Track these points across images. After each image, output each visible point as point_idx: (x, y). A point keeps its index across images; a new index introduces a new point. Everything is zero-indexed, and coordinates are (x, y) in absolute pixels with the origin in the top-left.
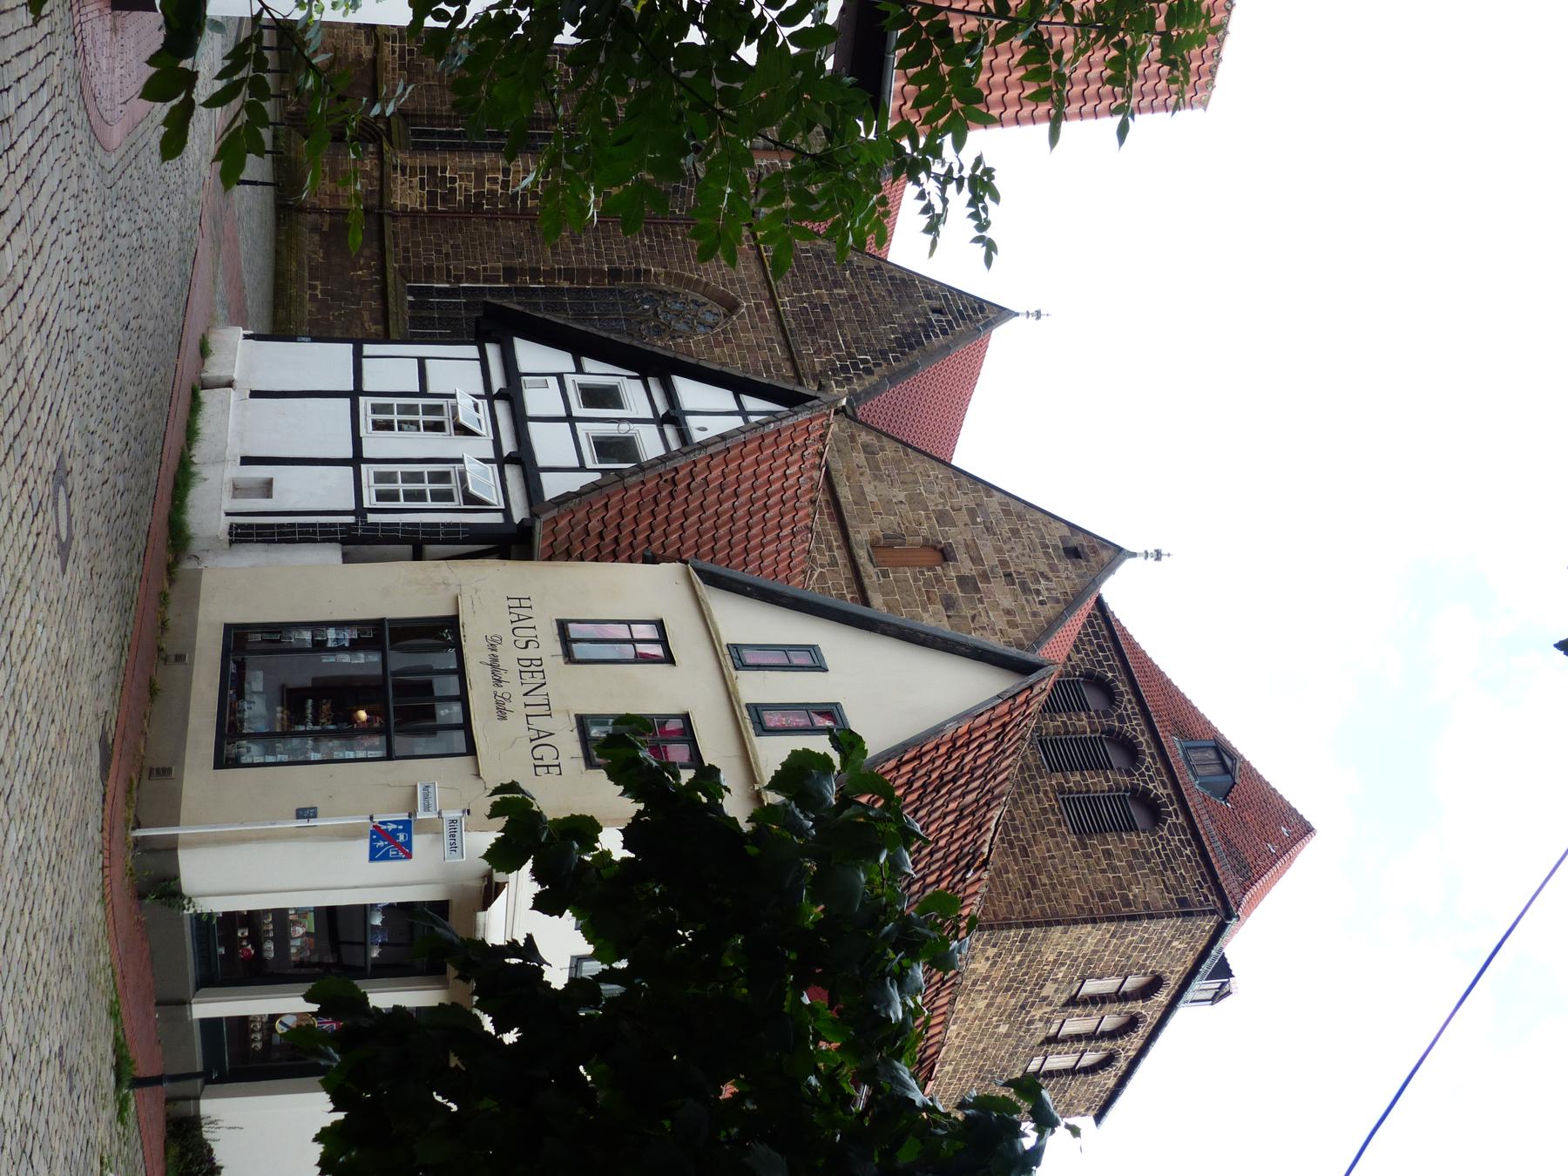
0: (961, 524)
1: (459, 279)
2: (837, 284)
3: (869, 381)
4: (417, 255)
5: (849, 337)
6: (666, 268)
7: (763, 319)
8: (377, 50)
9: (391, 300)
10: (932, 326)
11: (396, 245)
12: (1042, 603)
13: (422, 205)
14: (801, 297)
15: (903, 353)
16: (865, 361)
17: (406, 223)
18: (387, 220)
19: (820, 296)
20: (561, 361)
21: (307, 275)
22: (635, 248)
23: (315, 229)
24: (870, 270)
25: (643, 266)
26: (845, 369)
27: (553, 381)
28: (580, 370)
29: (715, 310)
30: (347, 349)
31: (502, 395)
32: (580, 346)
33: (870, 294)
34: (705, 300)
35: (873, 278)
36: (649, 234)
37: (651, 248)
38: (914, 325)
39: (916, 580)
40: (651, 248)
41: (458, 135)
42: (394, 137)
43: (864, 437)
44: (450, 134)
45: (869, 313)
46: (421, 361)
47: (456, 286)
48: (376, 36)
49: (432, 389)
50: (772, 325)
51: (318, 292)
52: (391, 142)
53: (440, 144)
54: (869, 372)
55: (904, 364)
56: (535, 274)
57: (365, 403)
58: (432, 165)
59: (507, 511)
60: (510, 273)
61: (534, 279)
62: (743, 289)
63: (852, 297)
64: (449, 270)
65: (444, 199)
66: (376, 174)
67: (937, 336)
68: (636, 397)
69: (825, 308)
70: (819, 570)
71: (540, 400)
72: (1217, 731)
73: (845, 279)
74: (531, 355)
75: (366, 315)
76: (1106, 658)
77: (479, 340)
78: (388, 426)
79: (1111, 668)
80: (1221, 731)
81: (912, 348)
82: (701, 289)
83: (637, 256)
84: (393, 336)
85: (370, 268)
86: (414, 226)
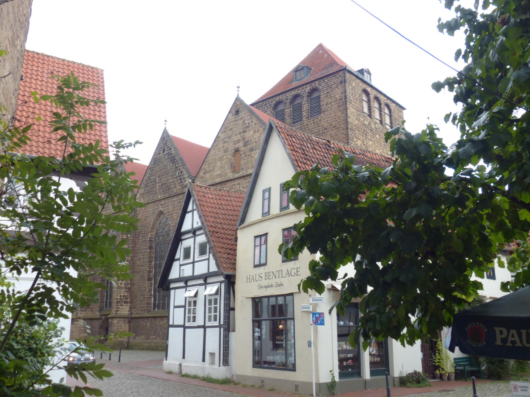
0: (228, 146)
1: (151, 295)
2: (155, 181)
3: (184, 172)
4: (143, 307)
5: (171, 178)
6: (149, 232)
7: (165, 203)
8: (80, 318)
9: (157, 315)
10: (168, 153)
11: (140, 313)
12: (252, 122)
13: (128, 305)
14: (159, 192)
15: (176, 162)
16: (179, 173)
17: (133, 311)
18: (132, 316)
19: (159, 186)
20: (176, 265)
21: (148, 341)
22: (143, 241)
23: (134, 338)
24: (151, 171)
25: (148, 239)
26: (181, 179)
27: (182, 268)
29: (162, 218)
30: (171, 330)
32: (171, 259)
33: (158, 171)
34: (159, 222)
35: (153, 170)
36: (138, 237)
37: (143, 237)
38: (168, 158)
39: (244, 159)
40: (143, 237)
41: (107, 294)
43: (201, 174)
44: (107, 297)
45: (164, 172)
47: (153, 296)
48: (76, 318)
50: (167, 201)
51: (154, 337)
52: (109, 315)
53: (110, 299)
54: (182, 172)
55: (180, 162)
56: (150, 272)
57: (187, 324)
58: (116, 302)
59: (221, 282)
60: (149, 279)
61: (151, 272)
62: (156, 209)
63: (159, 177)
64: (148, 298)
65: (126, 299)
66: (118, 319)
67: (171, 152)
68: (187, 243)
69: (162, 185)
70: (241, 188)
71: (187, 271)
72: (291, 71)
73: (154, 179)
74: (174, 274)
75: (161, 323)
76: (269, 103)
81: (175, 159)
82: (156, 222)
83: (145, 241)
85: (147, 322)
86: (135, 308)
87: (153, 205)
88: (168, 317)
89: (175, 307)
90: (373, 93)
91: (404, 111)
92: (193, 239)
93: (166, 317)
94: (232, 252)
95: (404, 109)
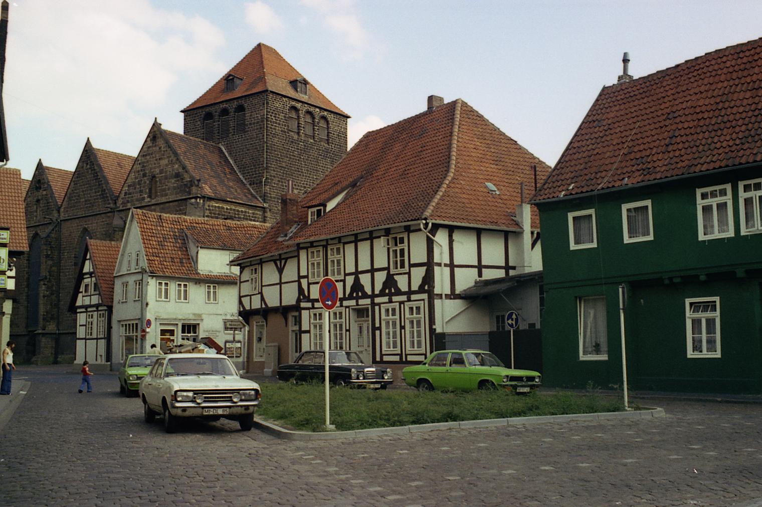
20: (80, 295)
27: (84, 298)
28: (82, 292)
30: (78, 341)
31: (86, 309)
32: (77, 292)
38: (91, 174)
40: (68, 252)
42: (34, 329)
46: (80, 326)
49: (263, 288)
52: (36, 331)
57: (87, 337)
59: (106, 310)
68: (87, 281)
71: (87, 301)
72: (221, 79)
74: (79, 303)
77: (76, 313)
78: (91, 333)
79: (202, 112)
80: (221, 77)
84: (73, 331)
87: (77, 221)
88: (75, 333)
89: (80, 326)
90: (303, 109)
91: (348, 119)
92: (90, 279)
93: (73, 333)
94: (111, 290)
95: (349, 117)
